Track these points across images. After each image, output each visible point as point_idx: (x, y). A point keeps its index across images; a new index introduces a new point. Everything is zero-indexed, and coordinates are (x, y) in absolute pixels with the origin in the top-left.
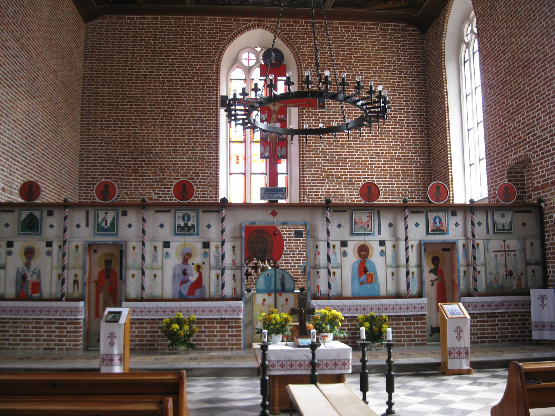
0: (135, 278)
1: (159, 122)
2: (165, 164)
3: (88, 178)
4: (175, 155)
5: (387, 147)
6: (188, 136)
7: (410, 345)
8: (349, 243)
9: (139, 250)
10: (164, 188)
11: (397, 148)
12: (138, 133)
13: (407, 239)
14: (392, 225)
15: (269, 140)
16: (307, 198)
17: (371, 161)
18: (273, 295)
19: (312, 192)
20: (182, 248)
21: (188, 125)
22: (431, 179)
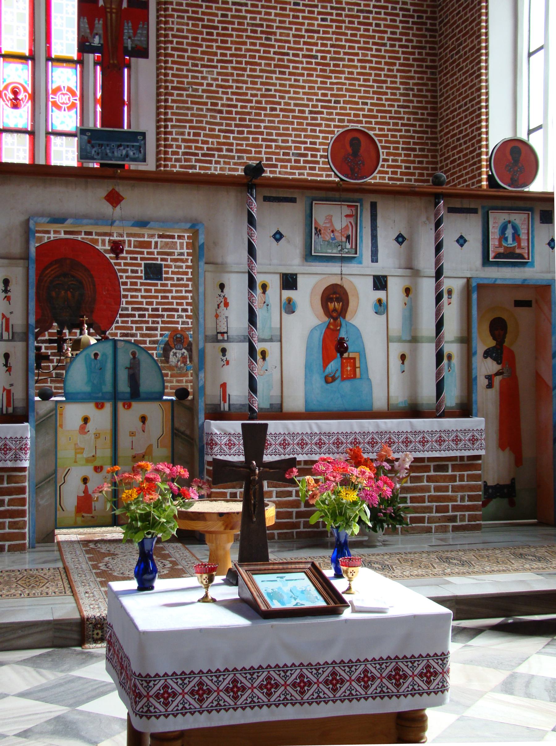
7: (444, 530)
8: (301, 280)
11: (368, 92)
13: (439, 273)
14: (404, 239)
17: (313, 118)
18: (108, 406)
22: (436, 163)
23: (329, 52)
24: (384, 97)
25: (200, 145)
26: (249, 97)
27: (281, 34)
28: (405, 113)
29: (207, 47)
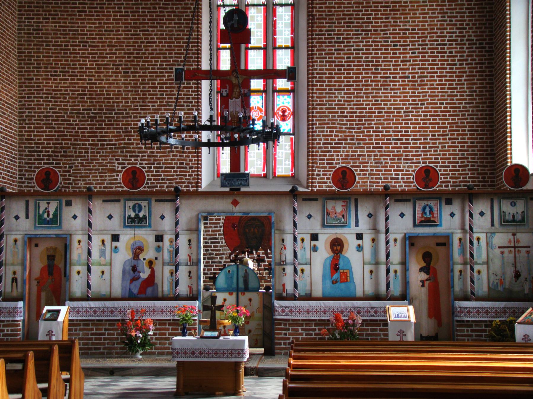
0: (81, 274)
1: (122, 69)
2: (131, 124)
3: (31, 144)
4: (144, 113)
5: (429, 96)
6: (161, 87)
8: (320, 237)
9: (84, 244)
10: (130, 156)
12: (95, 84)
13: (387, 231)
14: (372, 215)
15: (230, 119)
16: (317, 167)
17: (406, 116)
18: (235, 294)
19: (324, 160)
20: (132, 242)
21: (161, 72)
22: (493, 138)
23: (417, 73)
24: (455, 98)
25: (333, 138)
26: (364, 106)
27: (385, 65)
28: (470, 107)
29: (338, 78)
